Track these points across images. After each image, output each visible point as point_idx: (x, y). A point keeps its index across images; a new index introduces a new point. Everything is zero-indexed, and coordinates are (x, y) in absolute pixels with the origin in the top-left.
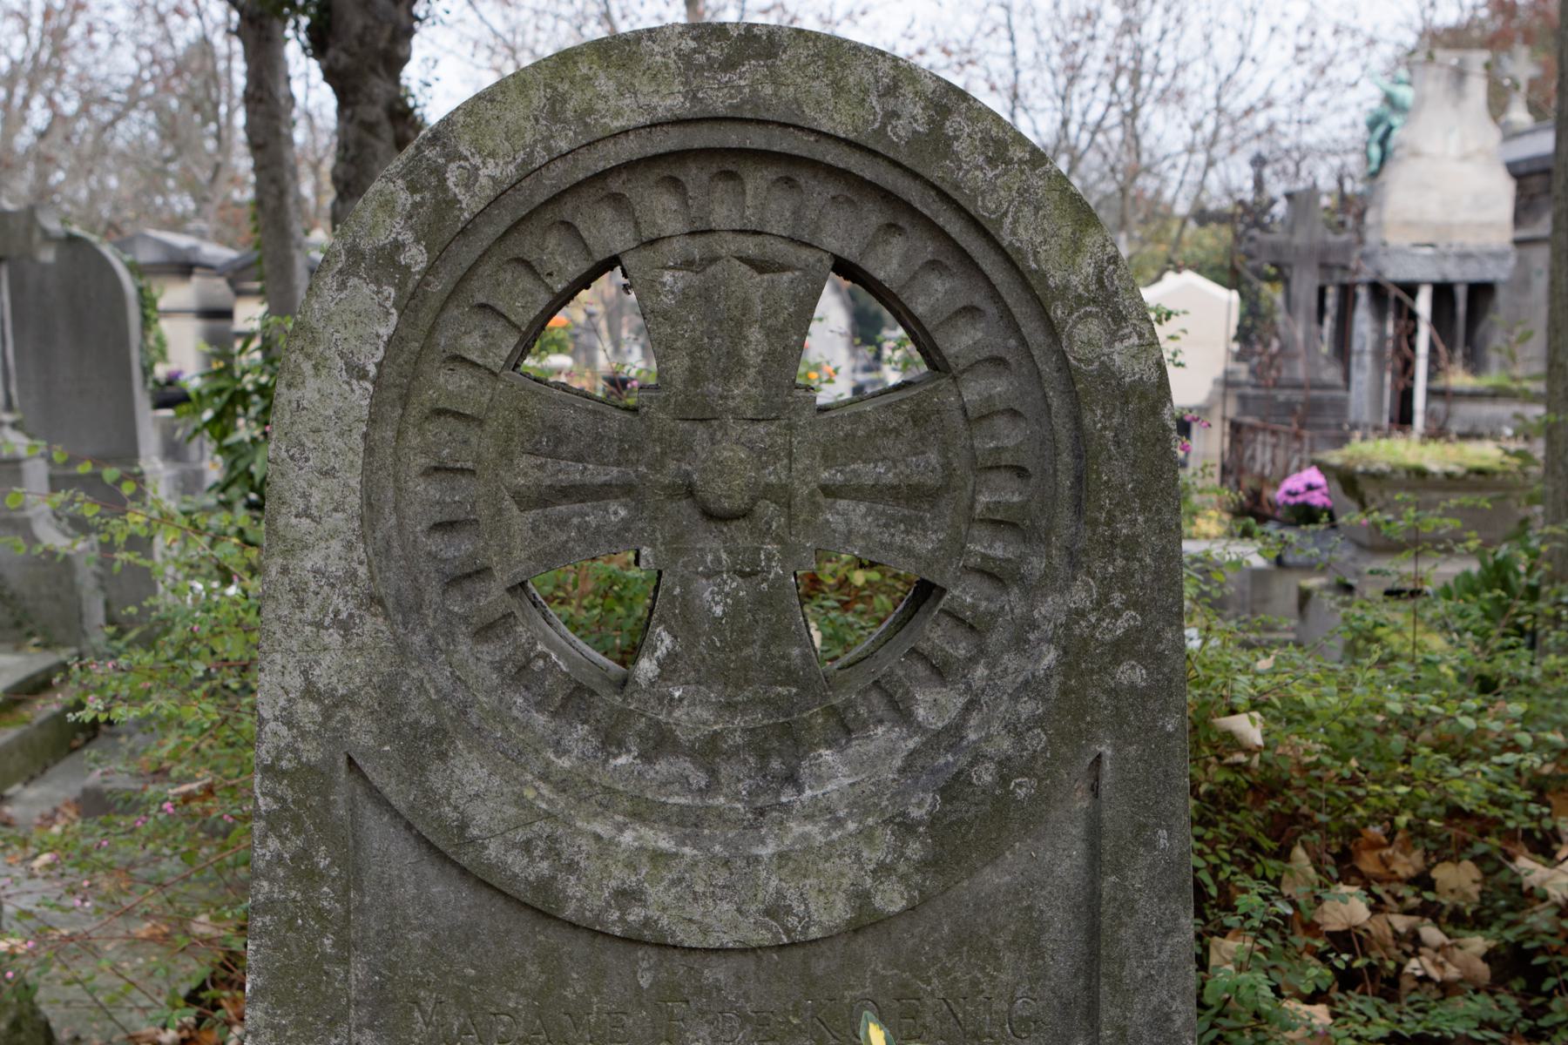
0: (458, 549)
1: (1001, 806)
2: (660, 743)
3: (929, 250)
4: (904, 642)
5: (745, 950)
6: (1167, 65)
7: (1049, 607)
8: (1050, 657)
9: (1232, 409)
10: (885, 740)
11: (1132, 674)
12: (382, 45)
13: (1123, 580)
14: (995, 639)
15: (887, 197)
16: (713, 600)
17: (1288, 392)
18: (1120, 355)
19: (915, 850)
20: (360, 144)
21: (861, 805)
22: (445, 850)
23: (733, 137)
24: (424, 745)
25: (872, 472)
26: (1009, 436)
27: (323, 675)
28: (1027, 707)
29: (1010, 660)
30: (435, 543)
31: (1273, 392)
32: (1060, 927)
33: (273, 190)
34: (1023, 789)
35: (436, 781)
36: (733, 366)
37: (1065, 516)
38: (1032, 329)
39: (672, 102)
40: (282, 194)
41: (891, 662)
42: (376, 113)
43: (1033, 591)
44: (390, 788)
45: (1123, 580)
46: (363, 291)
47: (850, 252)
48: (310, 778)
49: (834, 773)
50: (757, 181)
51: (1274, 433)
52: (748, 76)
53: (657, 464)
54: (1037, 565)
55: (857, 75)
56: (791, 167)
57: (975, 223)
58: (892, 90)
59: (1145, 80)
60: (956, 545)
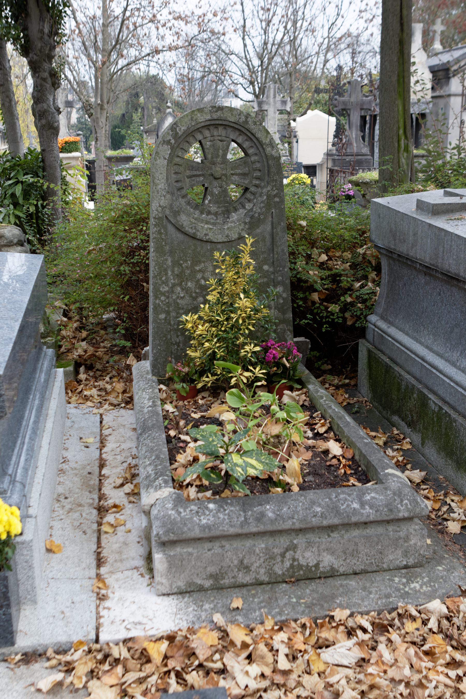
0: (179, 185)
1: (259, 219)
2: (209, 213)
3: (246, 138)
4: (244, 197)
5: (223, 242)
6: (308, 16)
7: (265, 190)
8: (265, 197)
9: (330, 165)
10: (242, 212)
11: (277, 199)
12: (47, 52)
13: (275, 186)
14: (257, 196)
15: (239, 130)
16: (216, 191)
17: (350, 157)
18: (274, 153)
19: (247, 226)
20: (42, 85)
21: (239, 221)
22: (179, 229)
23: (217, 122)
24: (176, 213)
25: (238, 171)
26: (258, 165)
27: (162, 204)
28: (262, 205)
29: (259, 198)
30: (175, 184)
31: (344, 158)
32: (268, 238)
33: (8, 100)
34: (262, 217)
35: (178, 219)
36: (217, 156)
37: (266, 177)
38: (261, 149)
39: (209, 117)
40: (11, 101)
41: (242, 200)
42: (46, 75)
43: (262, 188)
44: (172, 220)
45: (275, 186)
46: (165, 146)
47: (234, 138)
48: (160, 219)
49: (234, 216)
50: (220, 128)
51: (344, 173)
52: (219, 113)
53: (207, 171)
54: (263, 184)
55: (235, 113)
56: (225, 126)
57: (252, 134)
58: (240, 115)
59: (299, 25)
60: (251, 182)
